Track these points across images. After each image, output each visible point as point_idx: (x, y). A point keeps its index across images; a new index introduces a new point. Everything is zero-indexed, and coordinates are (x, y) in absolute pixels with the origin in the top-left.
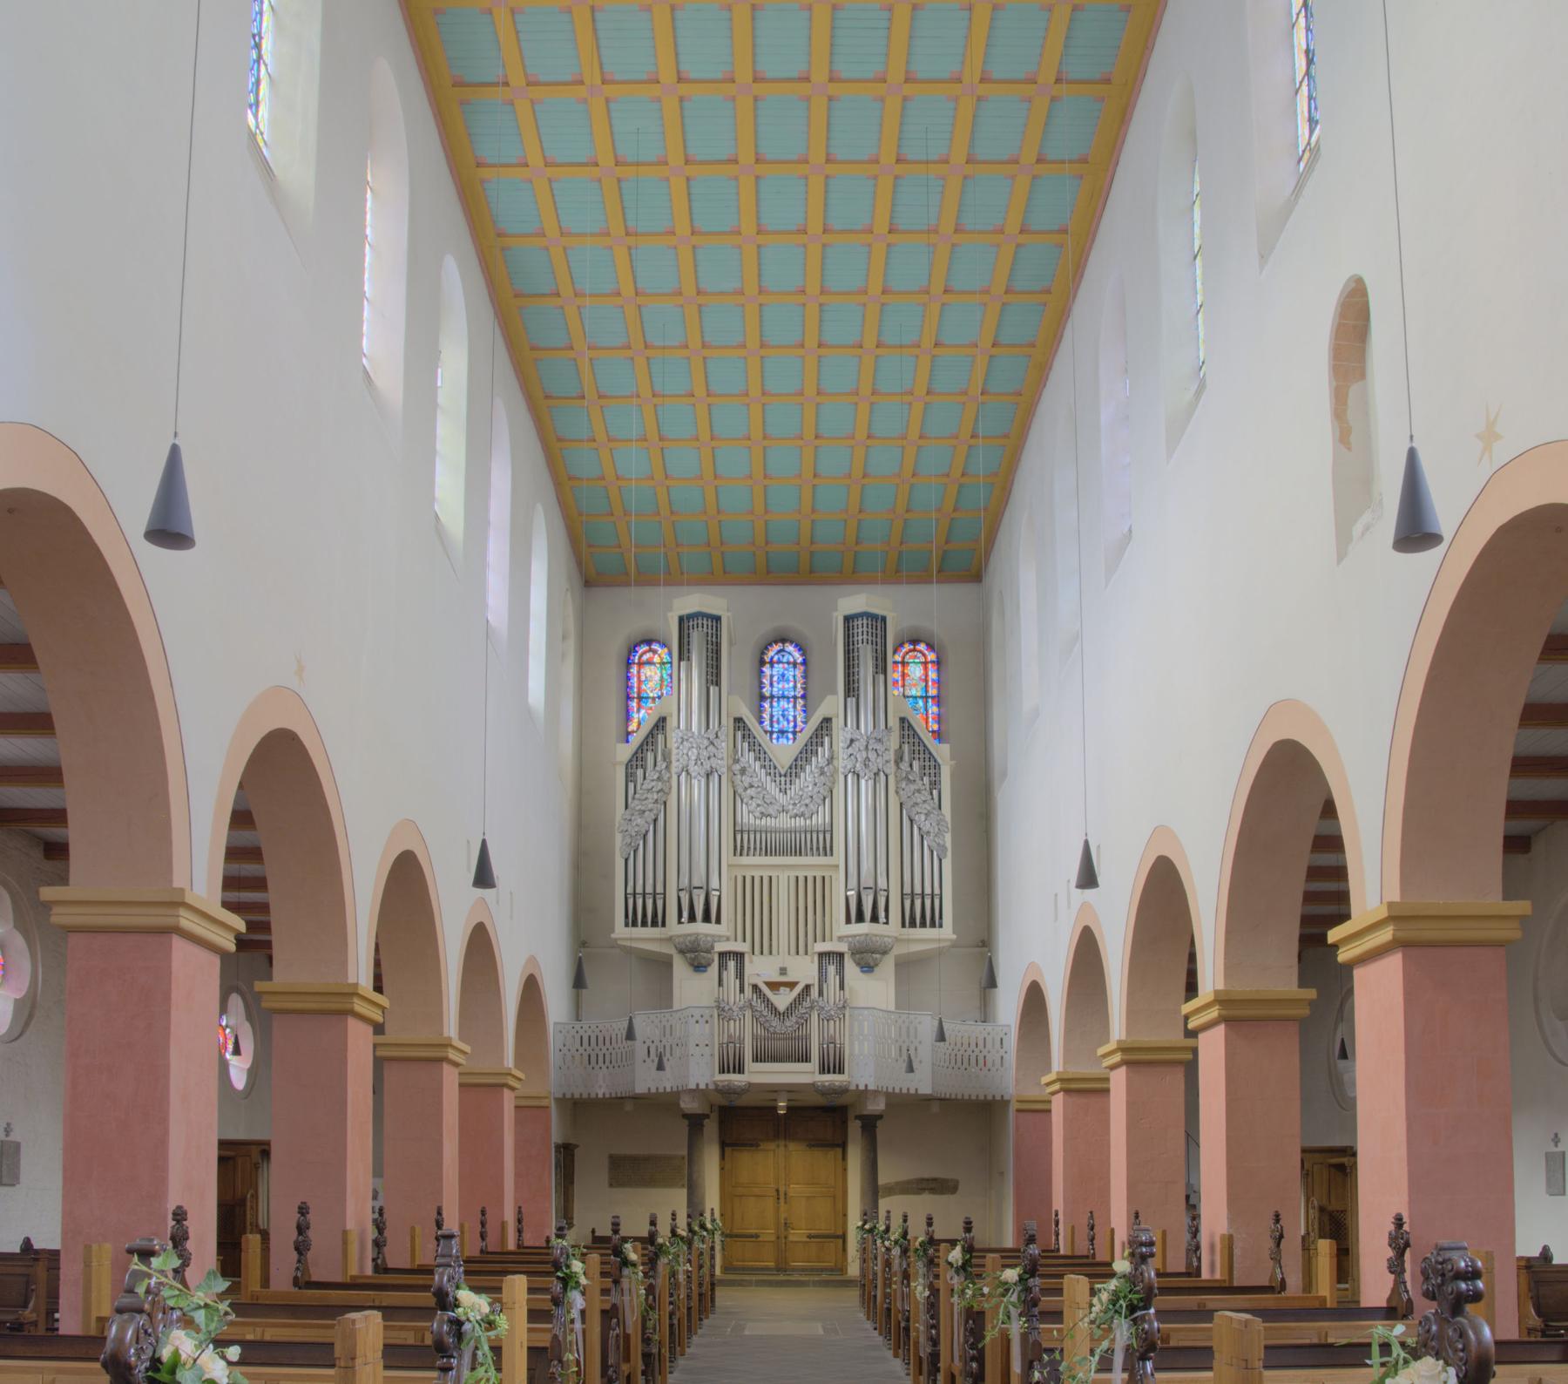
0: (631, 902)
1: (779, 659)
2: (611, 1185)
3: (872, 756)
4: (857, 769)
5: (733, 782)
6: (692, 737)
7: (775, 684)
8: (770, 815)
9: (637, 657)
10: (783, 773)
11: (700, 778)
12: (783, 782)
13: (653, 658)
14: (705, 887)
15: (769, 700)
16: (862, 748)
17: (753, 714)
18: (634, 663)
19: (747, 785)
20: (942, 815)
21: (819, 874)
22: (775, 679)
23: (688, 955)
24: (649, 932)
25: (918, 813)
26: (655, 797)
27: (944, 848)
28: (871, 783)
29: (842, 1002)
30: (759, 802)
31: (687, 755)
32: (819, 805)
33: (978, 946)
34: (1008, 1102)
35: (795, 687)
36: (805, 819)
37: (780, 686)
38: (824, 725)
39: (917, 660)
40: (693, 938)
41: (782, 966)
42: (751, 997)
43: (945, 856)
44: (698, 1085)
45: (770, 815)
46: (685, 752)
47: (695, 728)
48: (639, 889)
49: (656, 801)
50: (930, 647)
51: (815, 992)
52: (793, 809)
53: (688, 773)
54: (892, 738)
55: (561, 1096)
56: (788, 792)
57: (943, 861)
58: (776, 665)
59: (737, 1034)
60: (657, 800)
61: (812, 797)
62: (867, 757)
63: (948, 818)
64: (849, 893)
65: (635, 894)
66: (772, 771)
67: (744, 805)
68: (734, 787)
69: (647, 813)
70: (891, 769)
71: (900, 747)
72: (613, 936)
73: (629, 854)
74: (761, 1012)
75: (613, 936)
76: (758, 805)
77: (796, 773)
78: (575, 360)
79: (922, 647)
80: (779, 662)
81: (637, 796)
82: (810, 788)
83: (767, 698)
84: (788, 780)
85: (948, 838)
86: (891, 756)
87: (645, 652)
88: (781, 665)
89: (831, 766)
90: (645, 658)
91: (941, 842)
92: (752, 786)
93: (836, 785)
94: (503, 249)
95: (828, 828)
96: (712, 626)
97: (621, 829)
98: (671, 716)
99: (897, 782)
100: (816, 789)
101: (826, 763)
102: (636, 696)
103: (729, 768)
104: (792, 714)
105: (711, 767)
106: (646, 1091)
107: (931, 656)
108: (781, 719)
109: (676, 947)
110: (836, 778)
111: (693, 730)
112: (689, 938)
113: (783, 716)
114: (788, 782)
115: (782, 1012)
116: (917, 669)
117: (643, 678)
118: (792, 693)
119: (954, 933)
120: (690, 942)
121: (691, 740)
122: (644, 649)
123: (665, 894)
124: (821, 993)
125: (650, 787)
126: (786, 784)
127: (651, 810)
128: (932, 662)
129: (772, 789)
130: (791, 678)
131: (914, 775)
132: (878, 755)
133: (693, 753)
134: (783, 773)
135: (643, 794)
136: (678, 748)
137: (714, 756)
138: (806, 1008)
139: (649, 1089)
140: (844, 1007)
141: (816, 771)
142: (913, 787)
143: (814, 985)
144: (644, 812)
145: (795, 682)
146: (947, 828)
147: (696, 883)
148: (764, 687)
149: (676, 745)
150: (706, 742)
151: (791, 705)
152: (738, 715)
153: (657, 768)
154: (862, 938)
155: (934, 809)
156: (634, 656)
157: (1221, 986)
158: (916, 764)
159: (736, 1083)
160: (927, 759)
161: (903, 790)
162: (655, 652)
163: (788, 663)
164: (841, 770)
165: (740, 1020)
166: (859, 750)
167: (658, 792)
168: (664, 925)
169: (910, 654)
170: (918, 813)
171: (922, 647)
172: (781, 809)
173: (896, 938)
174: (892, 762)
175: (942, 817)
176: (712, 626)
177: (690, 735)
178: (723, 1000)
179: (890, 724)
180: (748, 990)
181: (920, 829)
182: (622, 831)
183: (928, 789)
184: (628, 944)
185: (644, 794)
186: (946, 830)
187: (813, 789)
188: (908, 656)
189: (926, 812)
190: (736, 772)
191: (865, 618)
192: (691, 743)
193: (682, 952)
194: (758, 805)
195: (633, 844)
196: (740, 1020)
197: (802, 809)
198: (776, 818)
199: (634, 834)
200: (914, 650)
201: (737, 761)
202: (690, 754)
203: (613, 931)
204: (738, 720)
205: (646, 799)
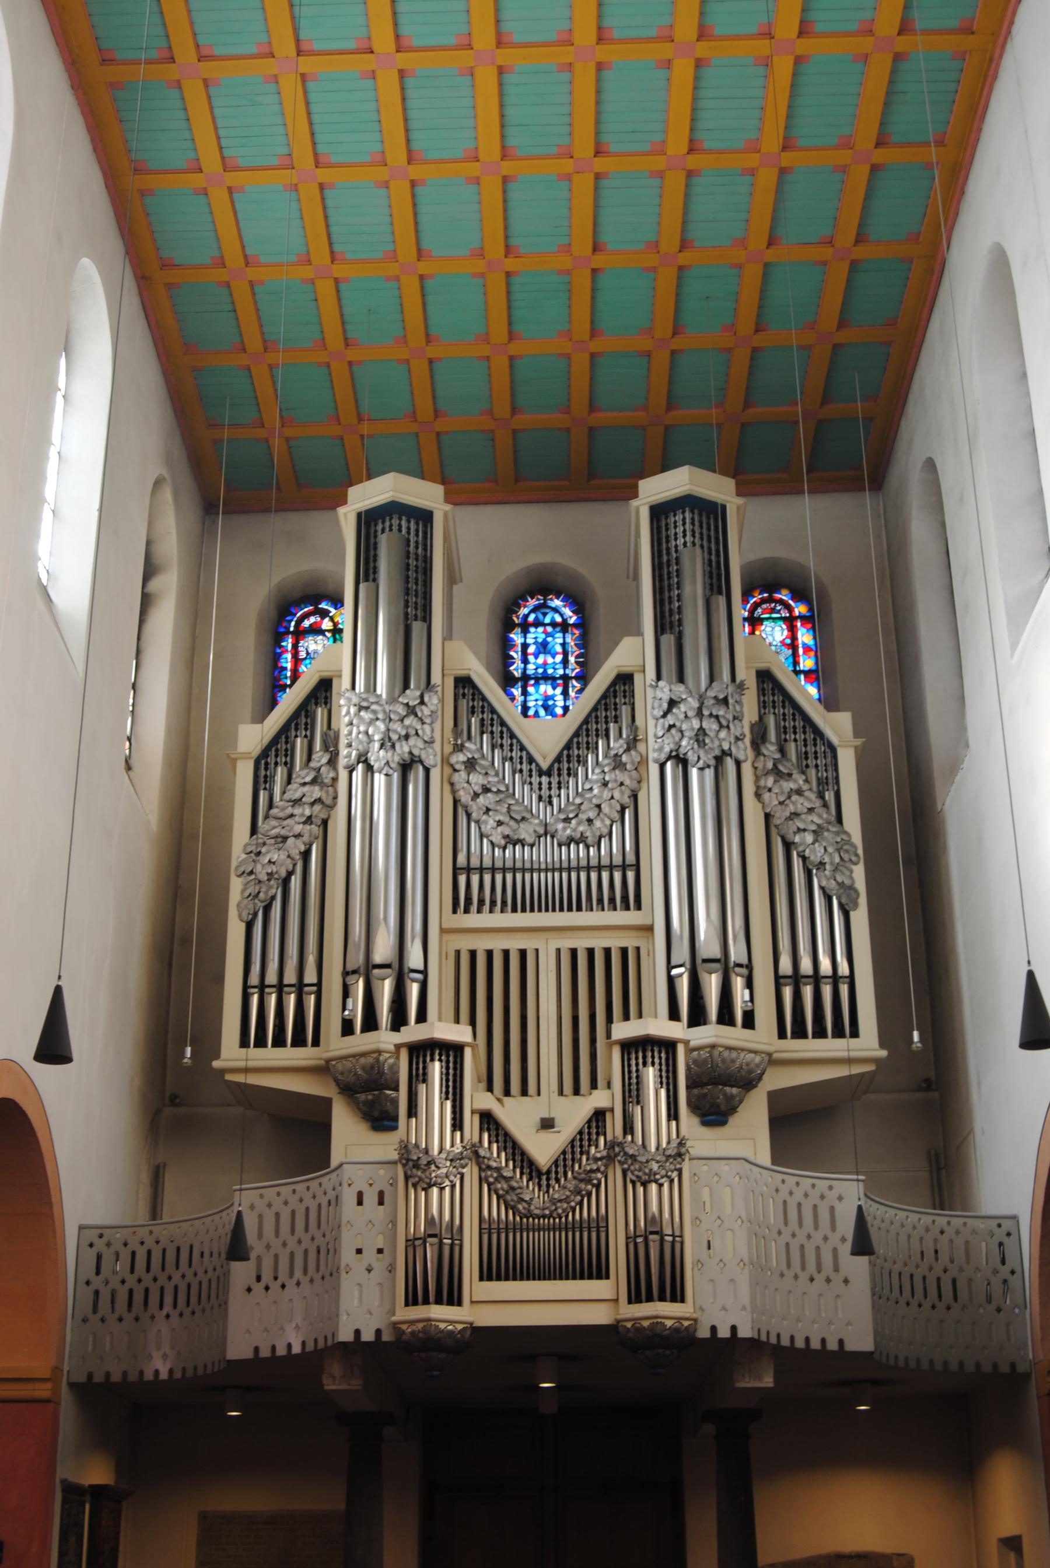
0: (255, 1000)
1: (536, 618)
3: (710, 725)
4: (682, 751)
5: (452, 784)
6: (377, 703)
7: (531, 658)
8: (522, 842)
9: (293, 624)
10: (545, 766)
11: (391, 772)
12: (545, 786)
13: (321, 623)
14: (396, 966)
15: (520, 684)
16: (690, 714)
17: (488, 669)
18: (288, 632)
19: (478, 789)
20: (846, 833)
21: (615, 942)
22: (531, 649)
23: (362, 1097)
24: (290, 1055)
25: (799, 830)
26: (307, 812)
27: (849, 889)
28: (709, 773)
29: (674, 1144)
30: (502, 818)
31: (367, 733)
32: (613, 822)
33: (919, 1089)
34: (1027, 1376)
35: (565, 662)
36: (587, 847)
37: (540, 660)
38: (620, 688)
39: (774, 615)
40: (370, 1060)
41: (546, 1116)
42: (476, 1139)
43: (856, 906)
44: (357, 1333)
45: (522, 842)
46: (362, 728)
47: (382, 688)
49: (309, 820)
50: (800, 595)
51: (615, 1126)
52: (565, 829)
53: (369, 768)
54: (745, 699)
55: (82, 1378)
56: (555, 801)
57: (852, 914)
58: (532, 630)
59: (447, 1217)
60: (310, 817)
61: (599, 806)
62: (701, 729)
63: (857, 838)
64: (674, 972)
65: (262, 987)
66: (525, 767)
67: (473, 825)
68: (454, 792)
69: (291, 841)
70: (744, 751)
71: (761, 718)
72: (216, 1064)
73: (255, 914)
74: (498, 1169)
75: (216, 1064)
76: (500, 823)
77: (569, 769)
78: (228, 285)
79: (784, 595)
80: (537, 624)
81: (274, 811)
82: (596, 791)
83: (516, 680)
84: (555, 780)
85: (859, 875)
86: (745, 728)
87: (306, 616)
88: (541, 629)
89: (633, 752)
90: (306, 623)
91: (847, 882)
92: (486, 790)
93: (644, 785)
94: (169, 286)
95: (630, 858)
96: (417, 531)
97: (242, 869)
98: (340, 676)
99: (757, 778)
100: (606, 795)
101: (625, 746)
103: (445, 760)
104: (562, 703)
105: (410, 753)
107: (800, 609)
108: (542, 712)
109: (338, 1085)
110: (644, 776)
111: (379, 692)
112: (363, 1060)
113: (546, 707)
114: (554, 785)
115: (545, 1169)
116: (778, 629)
117: (302, 654)
118: (561, 672)
119: (882, 1045)
120: (363, 1068)
121: (374, 707)
123: (319, 984)
124: (628, 1127)
125: (297, 795)
126: (550, 789)
127: (298, 836)
128: (802, 617)
129: (525, 794)
130: (559, 649)
131: (788, 765)
132: (721, 726)
133: (377, 728)
134: (545, 766)
135: (284, 809)
136: (351, 724)
137: (417, 734)
138: (596, 1160)
139: (257, 1349)
140: (680, 1155)
141: (606, 761)
142: (788, 785)
143: (612, 1110)
144: (285, 839)
145: (565, 654)
146: (857, 855)
147: (378, 958)
148: (513, 663)
149: (347, 719)
150: (402, 710)
151: (559, 690)
152: (462, 673)
153: (313, 764)
154: (705, 1054)
155: (829, 823)
158: (792, 749)
159: (442, 1326)
160: (810, 742)
161: (770, 790)
162: (324, 614)
163: (554, 624)
164: (652, 755)
165: (453, 1187)
166: (686, 717)
167: (313, 804)
168: (855, 1034)
169: (764, 606)
170: (799, 830)
171: (784, 595)
172: (541, 831)
173: (770, 1055)
174: (747, 740)
175: (844, 837)
176: (417, 531)
177: (372, 699)
178: (417, 1146)
179: (740, 675)
180: (472, 1124)
181: (804, 859)
183: (815, 788)
184: (239, 1078)
185: (285, 808)
186: (854, 858)
187: (601, 792)
188: (759, 610)
189: (813, 827)
190: (457, 767)
191: (687, 509)
192: (375, 712)
193: (348, 1090)
194: (500, 823)
195: (262, 895)
196: (453, 1187)
197: (581, 828)
198: (532, 846)
199: (264, 877)
200: (770, 600)
201: (459, 748)
202: (370, 732)
203: (217, 1056)
204: (464, 683)
205: (292, 816)
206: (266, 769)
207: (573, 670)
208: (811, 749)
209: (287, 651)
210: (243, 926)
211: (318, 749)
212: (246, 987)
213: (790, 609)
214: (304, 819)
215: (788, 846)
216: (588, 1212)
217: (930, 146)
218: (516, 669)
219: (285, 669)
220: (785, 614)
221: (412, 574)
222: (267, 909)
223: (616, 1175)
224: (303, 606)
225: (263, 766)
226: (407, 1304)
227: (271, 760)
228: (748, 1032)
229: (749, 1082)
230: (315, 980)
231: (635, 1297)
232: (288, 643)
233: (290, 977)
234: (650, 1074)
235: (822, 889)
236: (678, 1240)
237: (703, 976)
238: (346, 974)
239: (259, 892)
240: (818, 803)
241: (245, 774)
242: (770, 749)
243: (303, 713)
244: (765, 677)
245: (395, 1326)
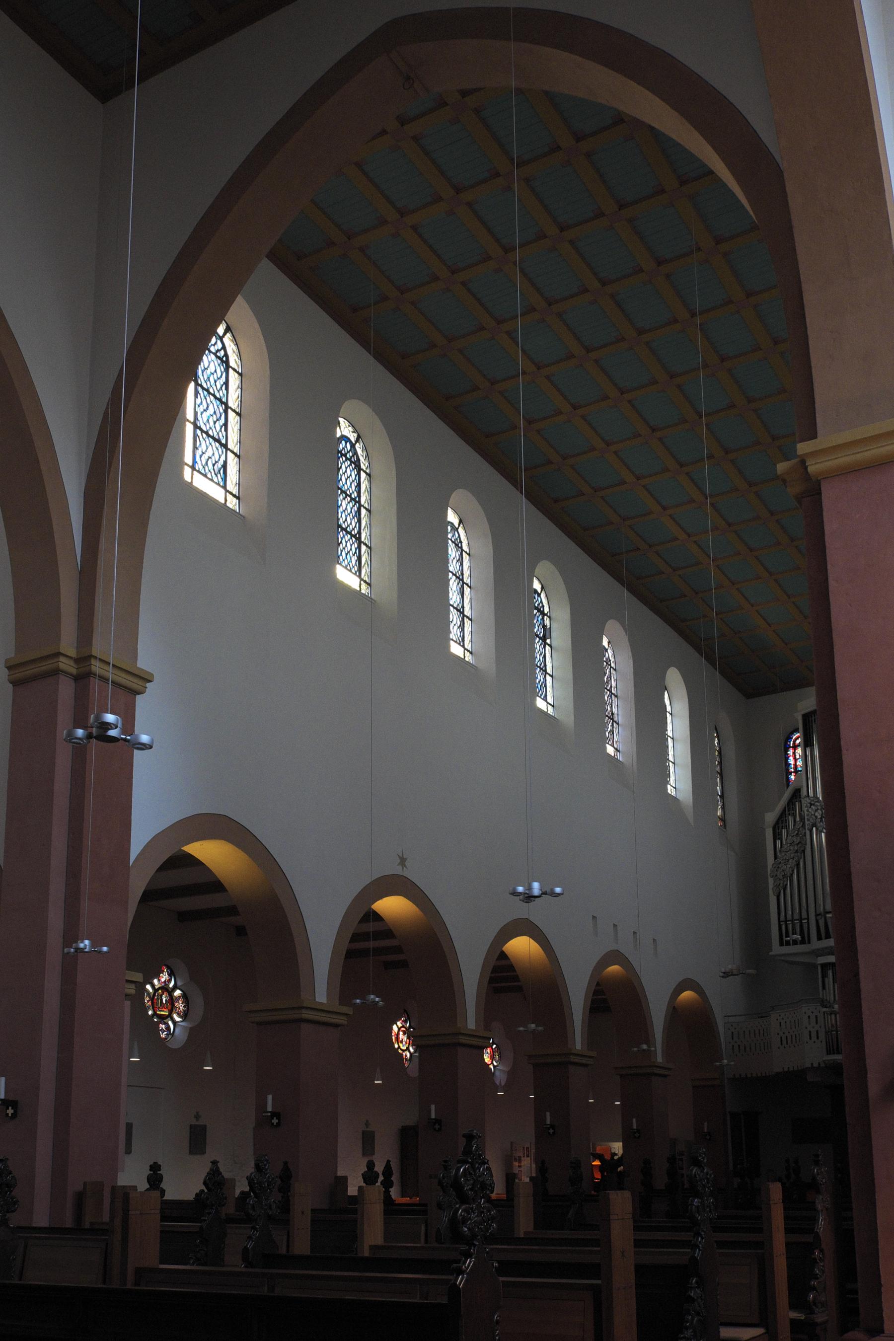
0: (784, 927)
2: (191, 1152)
9: (792, 743)
26: (796, 848)
48: (789, 917)
49: (797, 852)
60: (797, 850)
65: (786, 921)
69: (791, 861)
73: (780, 892)
102: (793, 770)
106: (782, 1071)
122: (797, 735)
144: (788, 860)
149: (806, 809)
156: (790, 742)
168: (809, 943)
178: (826, 1000)
182: (772, 877)
203: (771, 950)
206: (778, 829)
209: (790, 756)
210: (775, 897)
211: (798, 820)
212: (779, 921)
214: (794, 851)
219: (791, 764)
222: (785, 889)
224: (795, 733)
225: (777, 828)
226: (827, 1054)
227: (780, 825)
230: (806, 917)
232: (791, 752)
238: (817, 915)
239: (780, 884)
243: (791, 803)
245: (824, 1061)
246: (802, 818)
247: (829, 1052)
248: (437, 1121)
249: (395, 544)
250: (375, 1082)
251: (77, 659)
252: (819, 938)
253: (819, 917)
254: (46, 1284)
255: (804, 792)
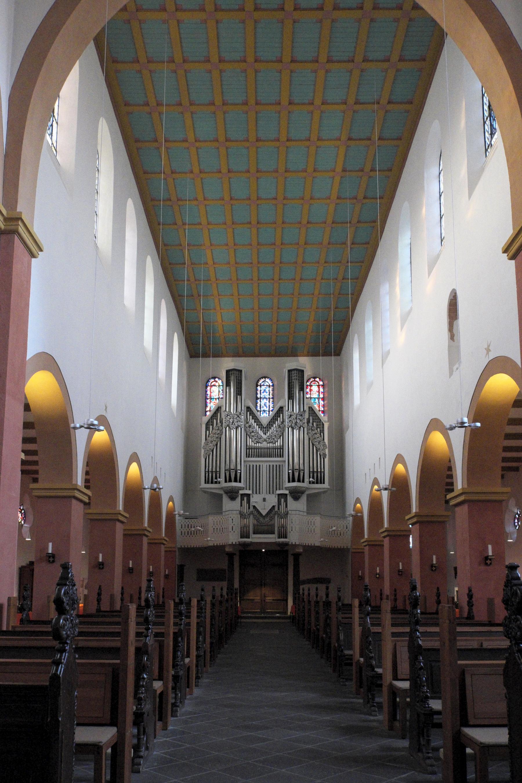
0: (207, 474)
3: (298, 421)
7: (262, 393)
10: (265, 427)
19: (251, 431)
21: (278, 464)
22: (262, 391)
23: (229, 494)
26: (217, 436)
35: (269, 394)
49: (217, 438)
51: (276, 509)
63: (327, 443)
65: (212, 472)
68: (246, 432)
74: (256, 516)
76: (255, 439)
80: (263, 385)
84: (267, 429)
85: (327, 451)
92: (253, 432)
99: (308, 430)
103: (245, 425)
107: (321, 383)
108: (264, 406)
113: (265, 405)
117: (212, 391)
119: (329, 485)
124: (279, 509)
127: (215, 441)
130: (268, 391)
134: (265, 427)
142: (314, 432)
151: (268, 401)
153: (218, 425)
157: (418, 511)
158: (315, 424)
162: (216, 382)
163: (267, 386)
168: (324, 483)
171: (317, 379)
181: (316, 447)
193: (226, 493)
194: (255, 439)
200: (315, 381)
207: (271, 396)
208: (319, 423)
213: (318, 383)
215: (313, 445)
216: (271, 523)
217: (379, 196)
218: (259, 396)
220: (318, 384)
221: (238, 384)
223: (276, 517)
228: (303, 483)
229: (303, 492)
231: (279, 538)
233: (214, 470)
234: (283, 500)
235: (320, 454)
236: (286, 528)
237: (295, 473)
238: (225, 470)
240: (320, 436)
241: (204, 426)
242: (311, 425)
244: (311, 409)
245: (239, 542)
246: (221, 422)
247: (241, 537)
248: (102, 564)
249: (111, 217)
250: (27, 539)
251: (7, 218)
252: (289, 482)
253: (226, 471)
254: (26, 684)
255: (223, 409)
